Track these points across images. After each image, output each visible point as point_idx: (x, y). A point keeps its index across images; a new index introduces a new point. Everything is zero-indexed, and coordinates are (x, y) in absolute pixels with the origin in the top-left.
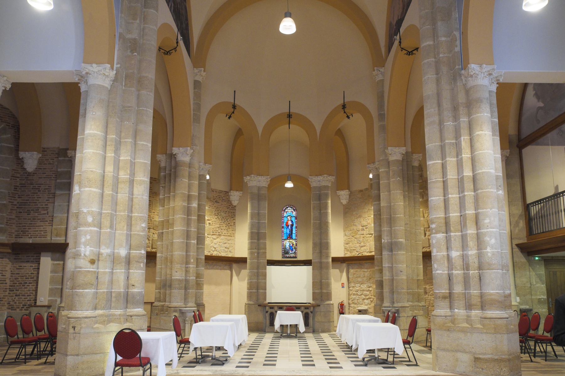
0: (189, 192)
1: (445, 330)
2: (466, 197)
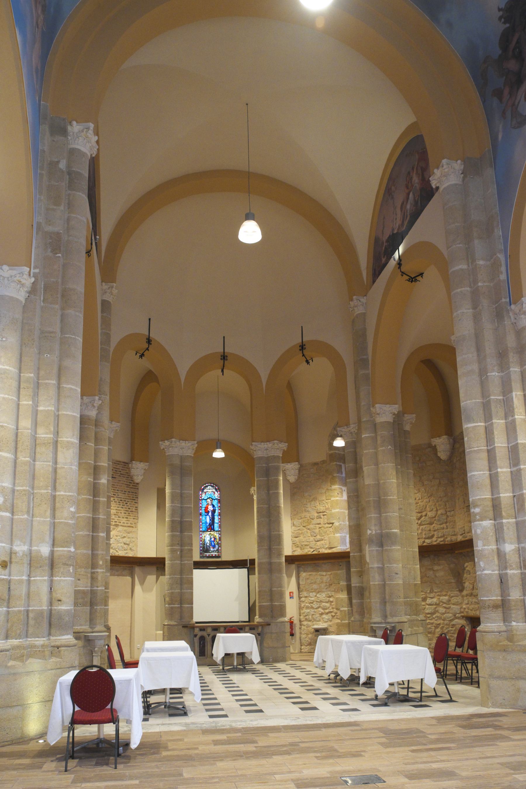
0: (95, 461)
1: (500, 651)
2: (522, 472)
